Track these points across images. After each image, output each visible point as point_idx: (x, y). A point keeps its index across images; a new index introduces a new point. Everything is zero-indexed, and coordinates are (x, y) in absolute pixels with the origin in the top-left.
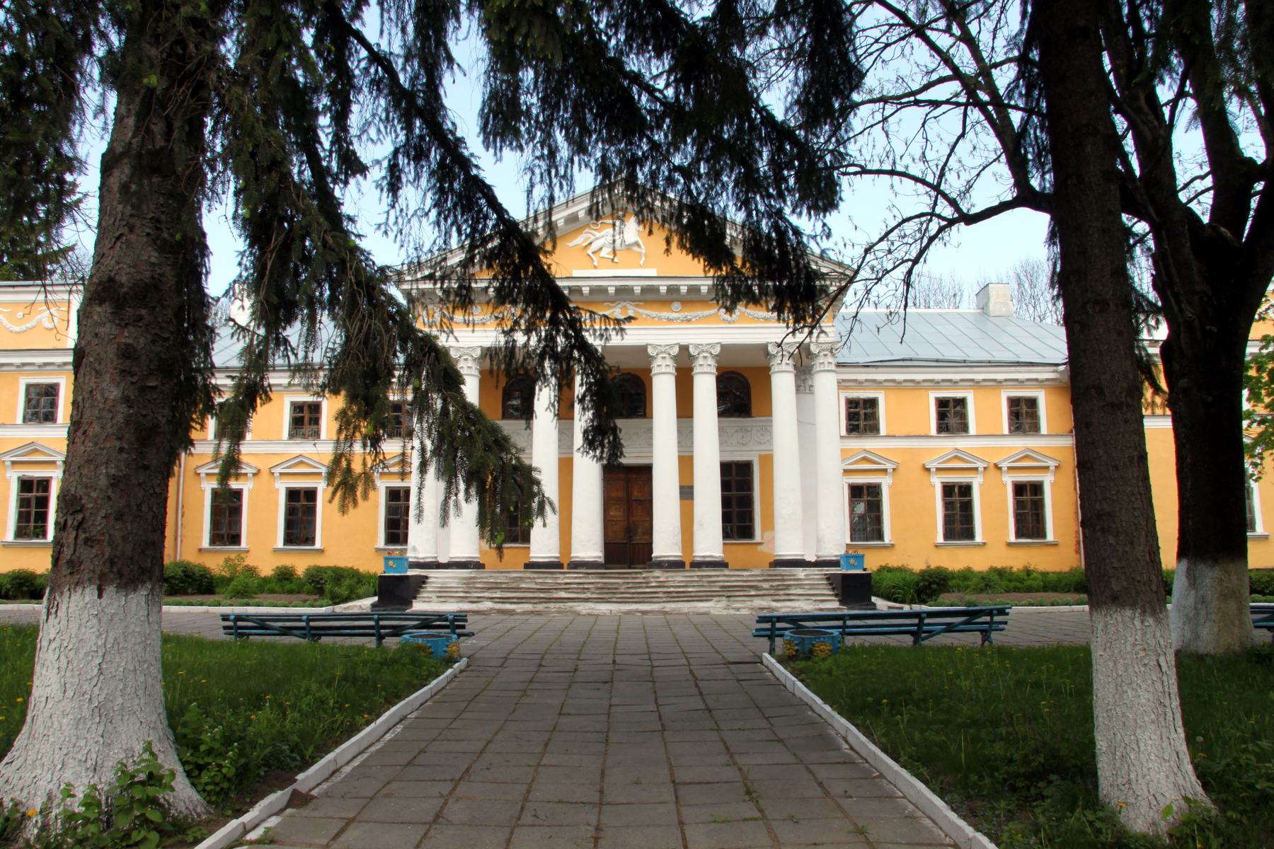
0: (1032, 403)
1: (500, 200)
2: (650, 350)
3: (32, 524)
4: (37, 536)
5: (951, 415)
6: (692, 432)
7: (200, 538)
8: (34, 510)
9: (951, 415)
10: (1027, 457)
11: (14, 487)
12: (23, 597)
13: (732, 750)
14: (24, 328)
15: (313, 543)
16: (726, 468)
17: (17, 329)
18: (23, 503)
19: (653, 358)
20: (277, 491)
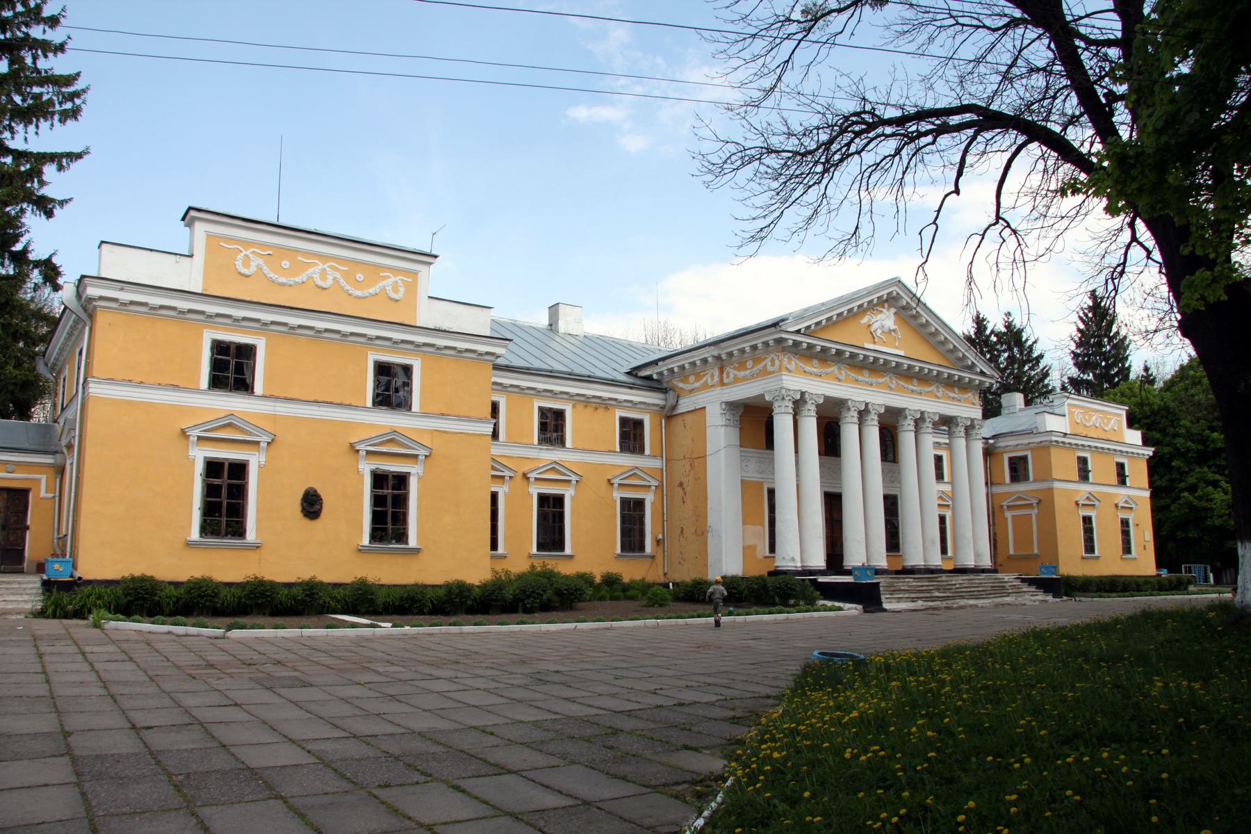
0: (639, 424)
1: (35, 151)
2: (767, 398)
3: (224, 519)
4: (556, 550)
5: (552, 427)
6: (840, 470)
7: (615, 548)
8: (390, 510)
9: (552, 427)
10: (230, 425)
11: (199, 468)
12: (207, 614)
13: (110, 700)
14: (366, 293)
15: (562, 549)
16: (886, 497)
17: (359, 293)
18: (378, 501)
19: (771, 404)
20: (193, 462)
